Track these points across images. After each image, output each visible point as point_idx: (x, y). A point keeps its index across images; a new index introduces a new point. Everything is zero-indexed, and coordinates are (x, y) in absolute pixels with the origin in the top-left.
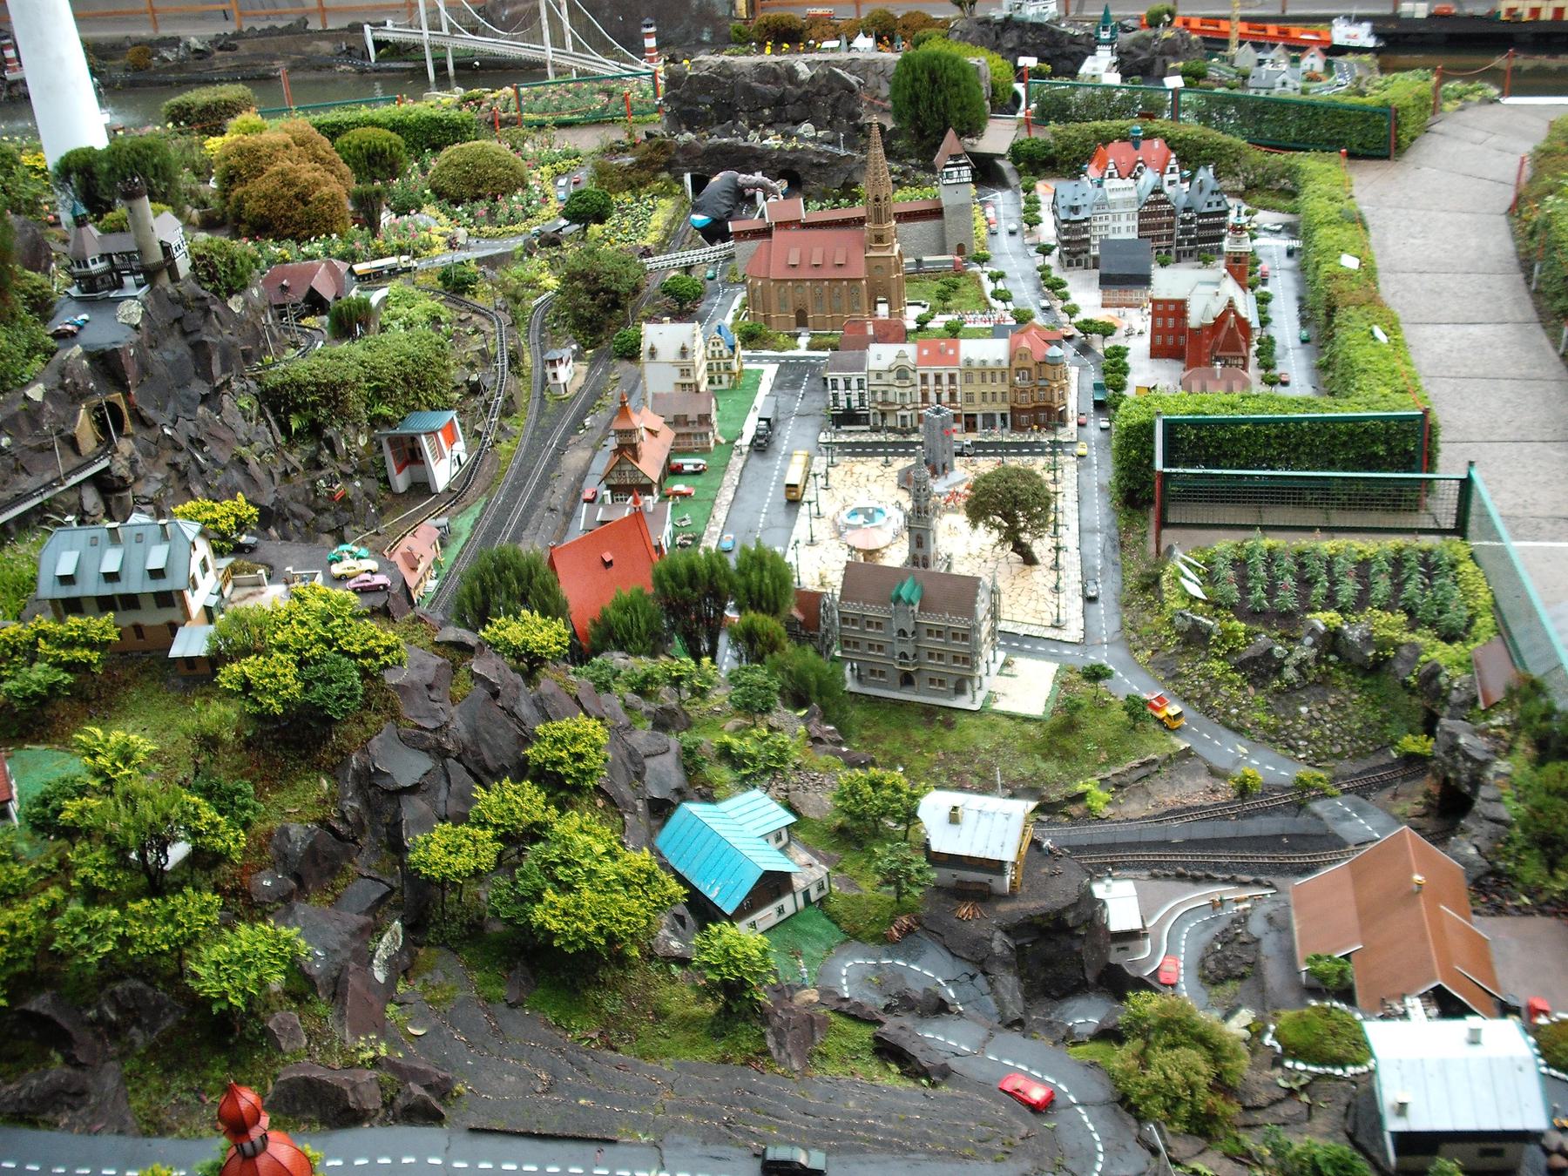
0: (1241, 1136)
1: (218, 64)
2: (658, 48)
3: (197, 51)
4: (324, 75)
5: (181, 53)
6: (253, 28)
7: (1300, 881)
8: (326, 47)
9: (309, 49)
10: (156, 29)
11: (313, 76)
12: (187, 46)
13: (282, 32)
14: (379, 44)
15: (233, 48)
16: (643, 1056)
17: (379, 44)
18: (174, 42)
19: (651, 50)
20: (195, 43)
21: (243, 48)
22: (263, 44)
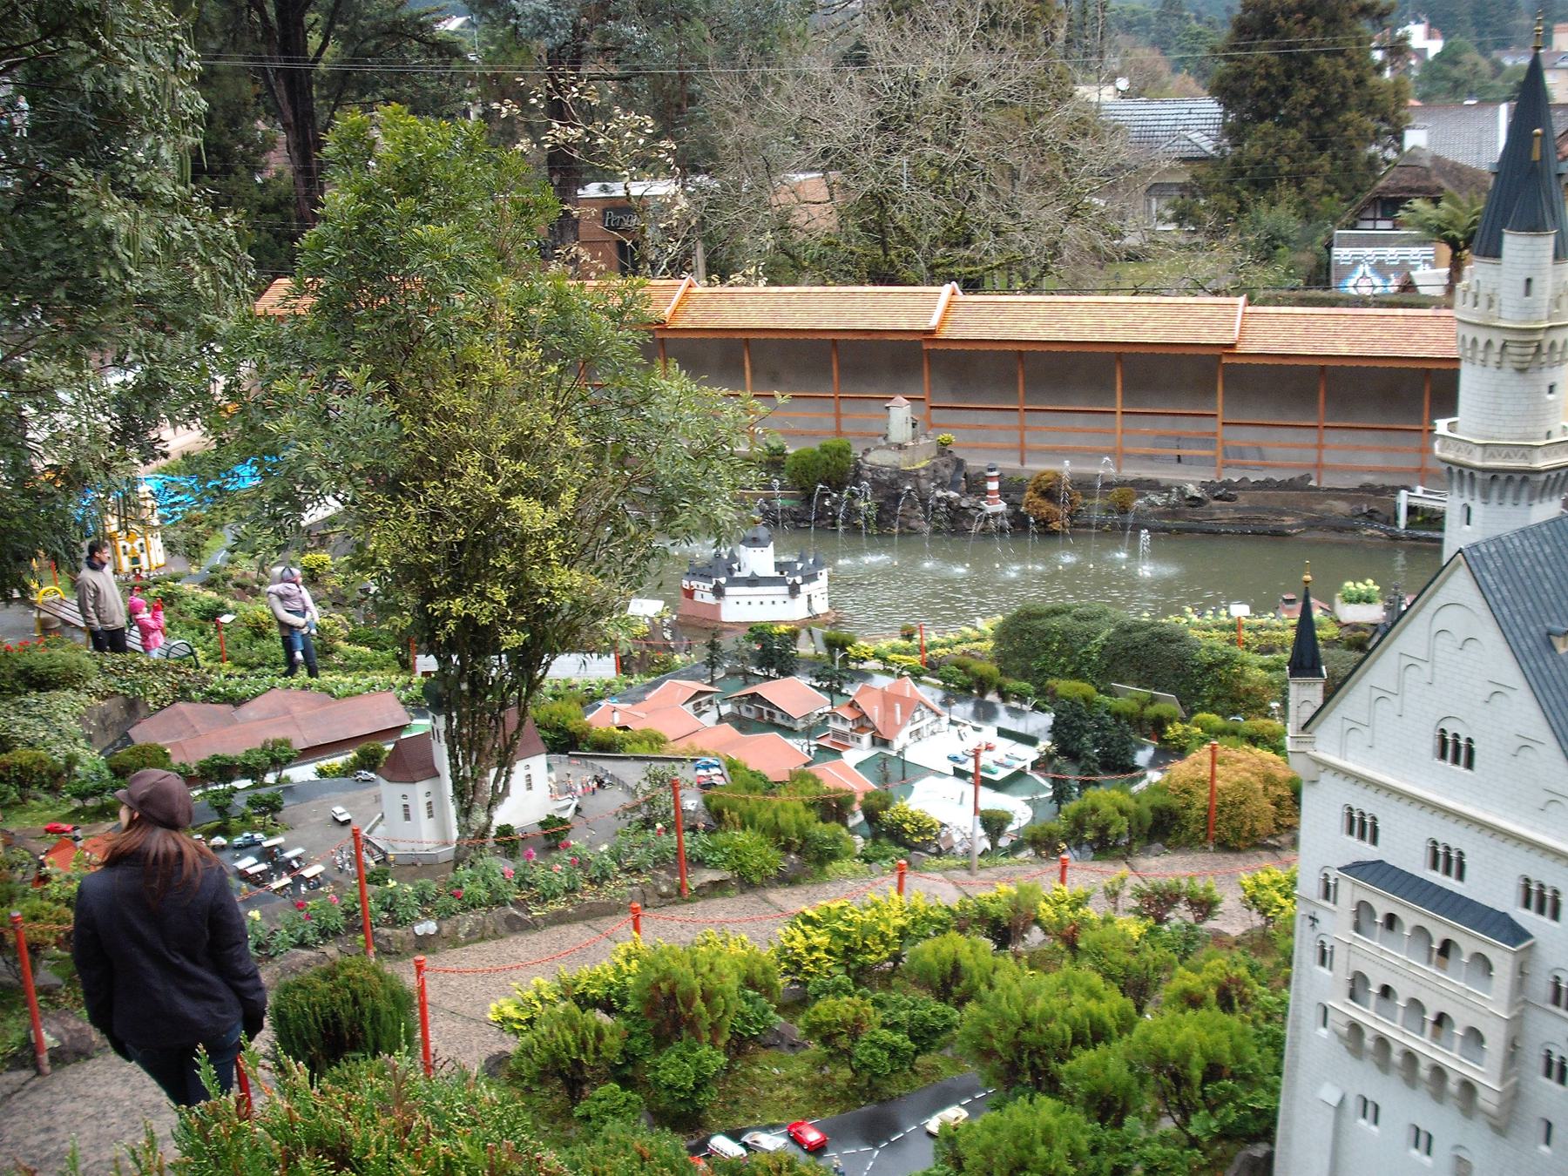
0: (773, 854)
1: (1218, 514)
2: (1000, 491)
3: (1193, 498)
4: (1347, 537)
5: (1174, 499)
6: (1244, 479)
7: (654, 692)
8: (1341, 507)
9: (1319, 507)
10: (1119, 469)
11: (1334, 537)
12: (1182, 492)
13: (1281, 486)
14: (1412, 510)
15: (1231, 499)
16: (160, 327)
17: (1412, 510)
18: (1154, 485)
19: (992, 492)
20: (1192, 490)
21: (1243, 500)
22: (1267, 497)
